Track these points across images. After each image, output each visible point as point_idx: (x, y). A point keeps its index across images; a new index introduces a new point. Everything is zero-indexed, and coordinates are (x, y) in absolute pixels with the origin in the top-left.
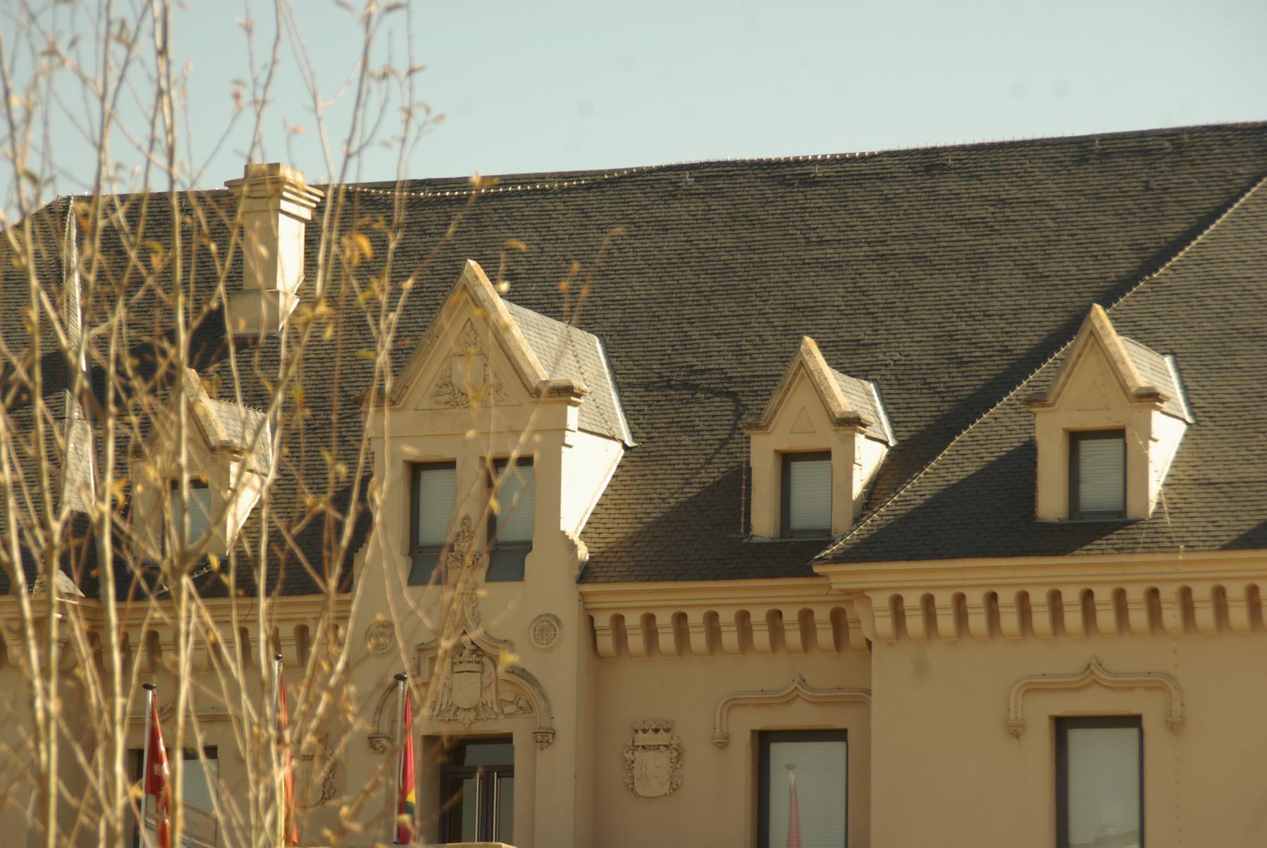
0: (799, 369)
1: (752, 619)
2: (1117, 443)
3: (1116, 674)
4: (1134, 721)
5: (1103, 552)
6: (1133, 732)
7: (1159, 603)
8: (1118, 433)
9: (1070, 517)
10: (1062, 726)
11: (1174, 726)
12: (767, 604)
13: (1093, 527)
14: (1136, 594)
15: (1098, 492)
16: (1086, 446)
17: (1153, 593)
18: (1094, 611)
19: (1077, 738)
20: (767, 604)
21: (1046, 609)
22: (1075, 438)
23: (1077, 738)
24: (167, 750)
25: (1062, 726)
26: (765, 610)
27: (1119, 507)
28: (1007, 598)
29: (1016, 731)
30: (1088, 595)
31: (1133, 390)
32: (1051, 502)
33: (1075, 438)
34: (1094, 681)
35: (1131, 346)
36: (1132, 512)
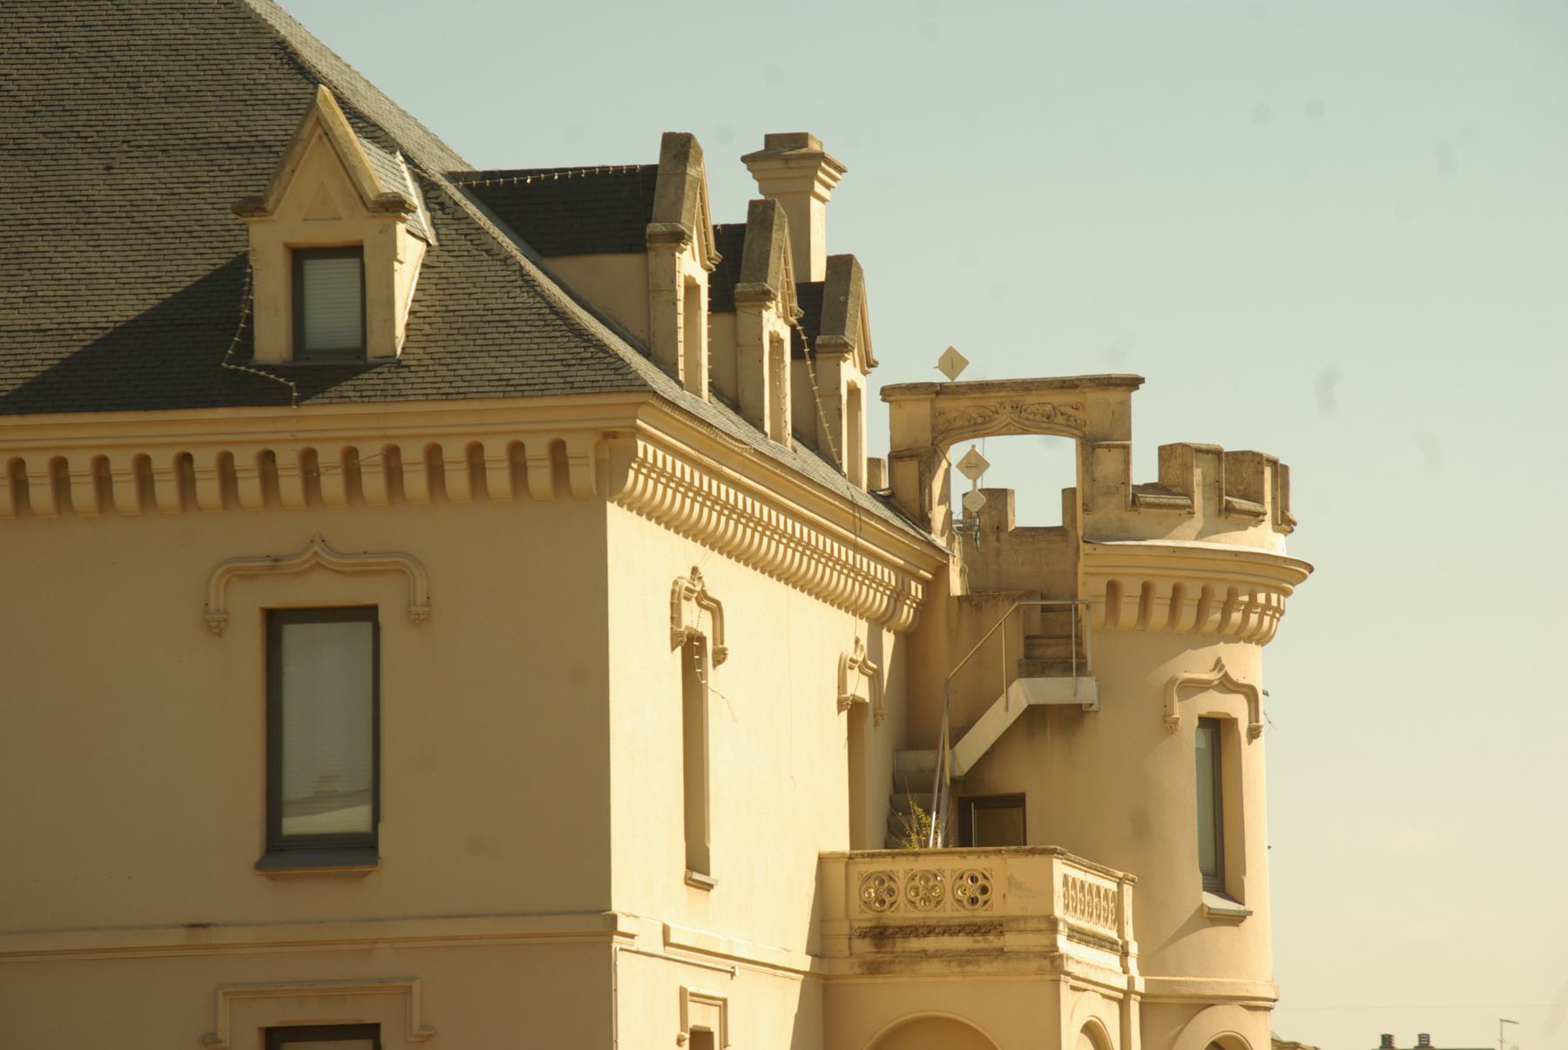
0: (314, 129)
1: (361, 457)
2: (351, 264)
3: (342, 555)
4: (368, 613)
5: (363, 398)
6: (365, 628)
7: (193, 473)
8: (355, 251)
9: (295, 358)
10: (275, 621)
11: (419, 618)
12: (380, 438)
13: (325, 370)
14: (454, 451)
15: (330, 322)
16: (313, 268)
17: (350, 454)
18: (193, 481)
19: (293, 635)
20: (380, 438)
21: (90, 479)
22: (300, 256)
23: (293, 635)
24: (1042, 598)
25: (275, 621)
26: (255, 450)
27: (355, 343)
28: (205, 460)
29: (216, 625)
30: (185, 460)
31: (372, 196)
32: (272, 340)
33: (300, 256)
34: (318, 565)
35: (365, 142)
36: (375, 349)
